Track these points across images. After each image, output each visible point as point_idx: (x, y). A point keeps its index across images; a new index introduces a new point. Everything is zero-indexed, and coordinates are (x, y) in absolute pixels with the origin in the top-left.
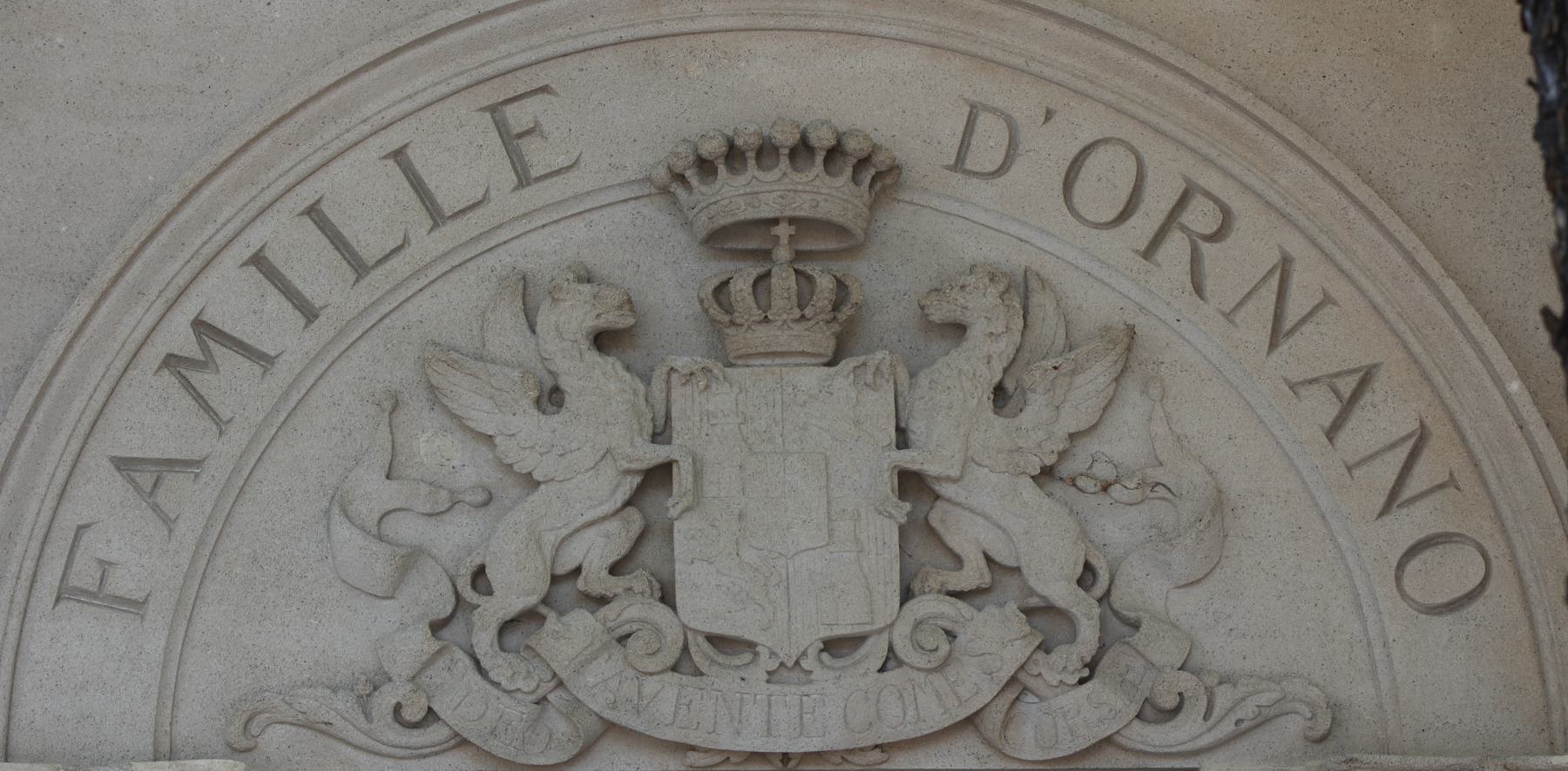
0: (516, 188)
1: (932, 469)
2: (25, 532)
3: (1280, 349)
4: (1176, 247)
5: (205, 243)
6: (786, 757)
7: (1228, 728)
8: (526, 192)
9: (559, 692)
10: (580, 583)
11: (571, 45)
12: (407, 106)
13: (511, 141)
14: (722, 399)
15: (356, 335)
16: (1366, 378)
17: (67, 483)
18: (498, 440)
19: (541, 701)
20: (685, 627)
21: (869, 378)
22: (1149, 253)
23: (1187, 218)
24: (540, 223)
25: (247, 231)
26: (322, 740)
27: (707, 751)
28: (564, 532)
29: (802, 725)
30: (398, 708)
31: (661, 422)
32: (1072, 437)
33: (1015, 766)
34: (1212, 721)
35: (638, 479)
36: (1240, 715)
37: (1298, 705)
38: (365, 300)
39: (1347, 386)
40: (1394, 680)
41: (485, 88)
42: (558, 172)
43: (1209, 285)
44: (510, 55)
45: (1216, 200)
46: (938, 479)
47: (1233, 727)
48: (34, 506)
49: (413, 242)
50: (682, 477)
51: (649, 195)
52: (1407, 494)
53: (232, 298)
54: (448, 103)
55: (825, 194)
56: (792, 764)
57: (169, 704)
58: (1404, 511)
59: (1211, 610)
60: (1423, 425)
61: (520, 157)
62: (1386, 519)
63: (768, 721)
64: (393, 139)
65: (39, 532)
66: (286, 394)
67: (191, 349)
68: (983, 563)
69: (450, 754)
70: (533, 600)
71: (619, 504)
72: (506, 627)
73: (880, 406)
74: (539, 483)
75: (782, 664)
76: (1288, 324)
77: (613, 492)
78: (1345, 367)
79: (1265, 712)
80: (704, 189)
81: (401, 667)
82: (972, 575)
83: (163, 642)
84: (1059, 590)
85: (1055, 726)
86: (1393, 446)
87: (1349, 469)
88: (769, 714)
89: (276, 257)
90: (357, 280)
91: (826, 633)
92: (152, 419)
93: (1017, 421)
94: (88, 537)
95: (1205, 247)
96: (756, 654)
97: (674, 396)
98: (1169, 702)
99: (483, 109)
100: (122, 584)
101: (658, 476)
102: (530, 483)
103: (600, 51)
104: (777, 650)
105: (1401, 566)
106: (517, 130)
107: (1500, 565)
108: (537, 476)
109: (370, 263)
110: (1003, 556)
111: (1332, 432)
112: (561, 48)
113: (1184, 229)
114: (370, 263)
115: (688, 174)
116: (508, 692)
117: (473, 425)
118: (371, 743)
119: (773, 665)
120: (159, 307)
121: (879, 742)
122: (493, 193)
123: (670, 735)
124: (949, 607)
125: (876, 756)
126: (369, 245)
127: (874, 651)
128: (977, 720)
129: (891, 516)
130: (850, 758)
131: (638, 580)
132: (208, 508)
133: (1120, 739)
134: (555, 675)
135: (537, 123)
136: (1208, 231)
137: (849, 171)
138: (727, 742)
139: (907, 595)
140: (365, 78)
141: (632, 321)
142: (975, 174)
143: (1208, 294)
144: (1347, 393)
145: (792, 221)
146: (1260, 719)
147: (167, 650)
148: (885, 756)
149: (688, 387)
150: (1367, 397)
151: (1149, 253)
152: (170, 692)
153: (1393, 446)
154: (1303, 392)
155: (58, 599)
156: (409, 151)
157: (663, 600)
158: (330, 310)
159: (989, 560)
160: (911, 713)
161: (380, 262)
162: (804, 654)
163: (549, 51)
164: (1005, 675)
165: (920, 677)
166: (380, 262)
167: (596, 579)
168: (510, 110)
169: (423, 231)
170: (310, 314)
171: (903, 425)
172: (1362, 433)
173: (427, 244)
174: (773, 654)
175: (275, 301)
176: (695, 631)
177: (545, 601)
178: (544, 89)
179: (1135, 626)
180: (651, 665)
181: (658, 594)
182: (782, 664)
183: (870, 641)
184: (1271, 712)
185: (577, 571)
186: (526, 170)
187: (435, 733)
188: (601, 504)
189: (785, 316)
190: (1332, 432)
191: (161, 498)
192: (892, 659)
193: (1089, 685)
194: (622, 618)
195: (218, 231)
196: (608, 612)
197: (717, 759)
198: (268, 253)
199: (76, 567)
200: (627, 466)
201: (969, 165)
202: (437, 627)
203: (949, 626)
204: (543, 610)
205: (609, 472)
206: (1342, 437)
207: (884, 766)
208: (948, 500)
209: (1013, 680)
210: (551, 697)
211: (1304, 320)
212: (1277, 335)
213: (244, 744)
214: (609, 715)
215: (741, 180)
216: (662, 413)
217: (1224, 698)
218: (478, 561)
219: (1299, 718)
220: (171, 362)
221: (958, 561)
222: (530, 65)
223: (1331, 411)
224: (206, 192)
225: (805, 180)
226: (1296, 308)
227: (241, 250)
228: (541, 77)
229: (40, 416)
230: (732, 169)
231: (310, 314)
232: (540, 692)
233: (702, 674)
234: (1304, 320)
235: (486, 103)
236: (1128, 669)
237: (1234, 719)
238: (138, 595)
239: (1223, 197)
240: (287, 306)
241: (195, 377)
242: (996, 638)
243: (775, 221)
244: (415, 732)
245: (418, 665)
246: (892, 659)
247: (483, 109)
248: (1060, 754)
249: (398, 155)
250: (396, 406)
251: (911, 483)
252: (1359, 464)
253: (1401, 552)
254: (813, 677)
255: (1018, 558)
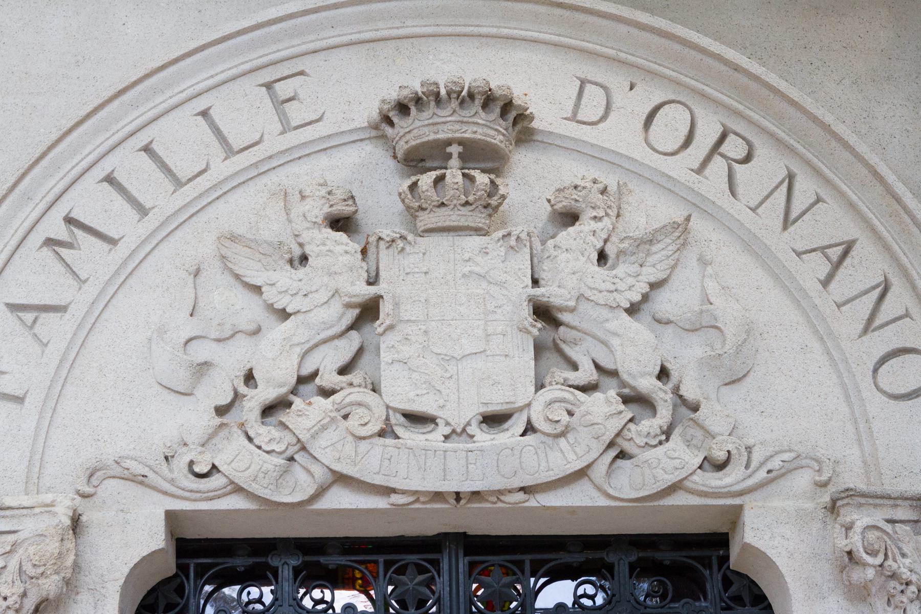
1: (556, 301)
3: (789, 230)
4: (718, 166)
5: (74, 167)
6: (458, 496)
7: (762, 475)
8: (288, 135)
9: (302, 453)
10: (318, 381)
12: (211, 82)
13: (280, 104)
15: (173, 227)
18: (263, 289)
19: (291, 459)
20: (388, 407)
22: (700, 170)
23: (724, 149)
24: (297, 156)
25: (102, 160)
26: (140, 490)
27: (404, 492)
28: (307, 346)
29: (468, 472)
30: (191, 463)
32: (654, 286)
34: (750, 470)
35: (357, 311)
36: (769, 466)
37: (808, 461)
38: (180, 203)
40: (874, 444)
42: (310, 123)
43: (740, 190)
44: (279, 51)
45: (744, 139)
47: (765, 475)
50: (385, 308)
51: (369, 138)
52: (877, 322)
53: (92, 202)
54: (238, 81)
55: (485, 128)
56: (463, 502)
57: (38, 465)
58: (876, 333)
59: (748, 399)
60: (886, 280)
61: (285, 114)
62: (864, 338)
63: (444, 470)
64: (201, 104)
67: (60, 231)
68: (593, 367)
69: (229, 497)
71: (344, 327)
73: (522, 262)
74: (290, 315)
75: (454, 431)
76: (793, 215)
77: (340, 318)
78: (832, 242)
82: (586, 374)
84: (647, 384)
86: (866, 292)
87: (839, 306)
88: (444, 464)
89: (120, 176)
91: (483, 409)
92: (35, 277)
93: (614, 272)
95: (736, 166)
96: (437, 424)
97: (381, 255)
98: (721, 455)
102: (284, 315)
103: (337, 50)
104: (450, 420)
105: (875, 371)
106: (284, 98)
108: (289, 310)
109: (184, 180)
113: (723, 156)
115: (391, 114)
116: (268, 452)
117: (247, 280)
118: (172, 489)
119: (447, 430)
120: (42, 206)
121: (522, 485)
122: (265, 137)
123: (378, 480)
125: (521, 496)
127: (518, 424)
129: (529, 332)
130: (502, 498)
131: (355, 377)
132: (69, 336)
133: (687, 483)
134: (299, 440)
136: (739, 157)
137: (498, 110)
139: (540, 386)
140: (182, 64)
141: (353, 209)
143: (740, 197)
146: (783, 470)
148: (526, 496)
149: (391, 250)
150: (848, 261)
151: (700, 170)
152: (38, 457)
153: (866, 292)
156: (211, 111)
157: (374, 390)
158: (156, 210)
159: (597, 367)
160: (543, 464)
161: (190, 180)
162: (469, 424)
163: (304, 48)
164: (607, 438)
165: (550, 441)
166: (190, 180)
167: (329, 378)
169: (220, 160)
170: (143, 211)
171: (536, 276)
172: (842, 286)
174: (447, 424)
175: (119, 201)
176: (395, 410)
177: (294, 392)
178: (302, 73)
179: (695, 408)
180: (364, 432)
181: (370, 387)
182: (454, 431)
183: (516, 415)
184: (794, 465)
185: (315, 374)
186: (288, 123)
187: (216, 481)
188: (331, 327)
189: (455, 202)
191: (37, 329)
192: (530, 429)
194: (345, 402)
195: (82, 159)
196: (336, 397)
197: (411, 499)
200: (347, 299)
201: (580, 117)
202: (221, 411)
203: (570, 407)
204: (292, 397)
205: (336, 307)
206: (833, 285)
207: (526, 504)
208: (568, 326)
209: (611, 444)
210: (296, 457)
211: (804, 213)
212: (787, 223)
213: (88, 490)
214: (337, 467)
215: (425, 115)
217: (757, 457)
218: (248, 367)
219: (809, 471)
220: (50, 242)
221: (575, 367)
222: (292, 58)
223: (826, 268)
224: (75, 134)
225: (468, 115)
226: (798, 206)
227: (100, 172)
228: (298, 65)
230: (420, 110)
231: (143, 211)
232: (289, 453)
233: (398, 438)
236: (693, 437)
238: (19, 393)
239: (749, 137)
242: (603, 407)
245: (206, 436)
246: (530, 429)
248: (647, 493)
249: (204, 114)
250: (197, 273)
251: (544, 313)
254: (475, 439)
255: (615, 363)
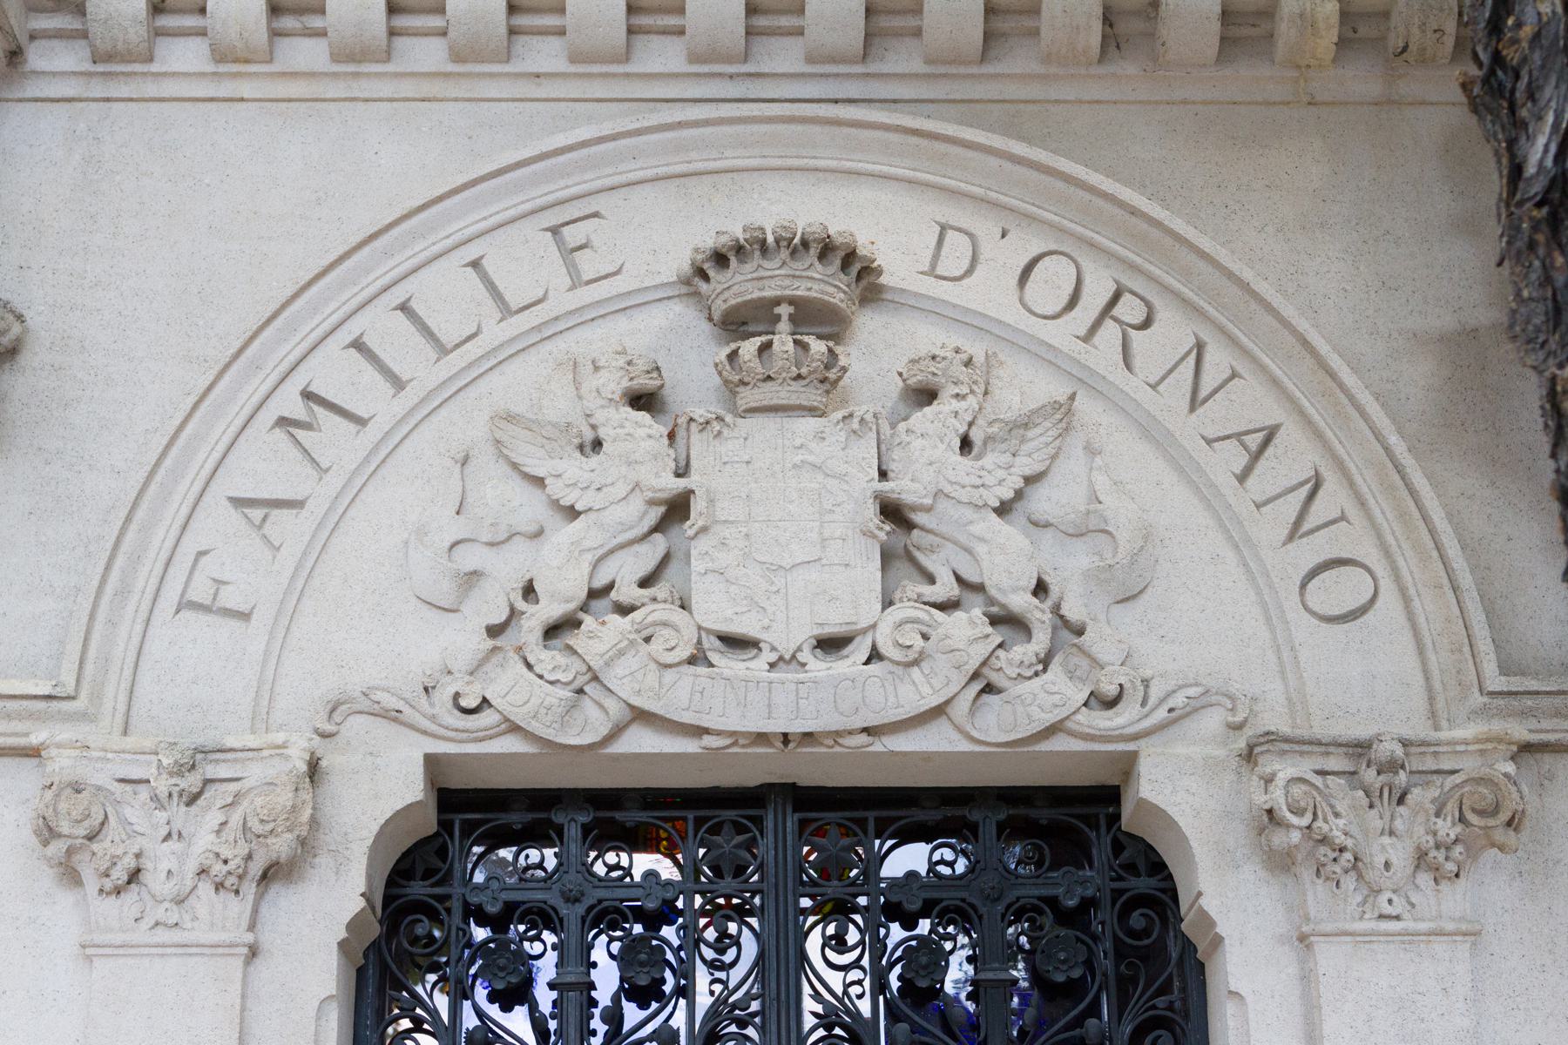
0: (570, 289)
1: (908, 498)
2: (152, 555)
4: (1110, 331)
7: (1161, 714)
8: (579, 291)
10: (613, 594)
11: (617, 180)
13: (570, 253)
14: (730, 447)
15: (436, 403)
16: (1270, 435)
17: (190, 517)
19: (580, 691)
21: (856, 426)
22: (1087, 338)
23: (1117, 311)
27: (719, 733)
30: (457, 696)
31: (683, 463)
32: (1030, 480)
33: (978, 748)
35: (662, 509)
36: (1171, 703)
39: (1254, 441)
41: (547, 213)
43: (1137, 362)
45: (1142, 299)
46: (914, 508)
48: (161, 533)
49: (484, 330)
50: (697, 506)
52: (1306, 527)
53: (336, 373)
54: (517, 224)
55: (821, 284)
57: (267, 697)
61: (575, 266)
62: (1289, 546)
64: (472, 252)
65: (164, 555)
66: (377, 447)
67: (297, 410)
70: (572, 606)
71: (646, 529)
72: (552, 631)
74: (579, 514)
76: (1203, 393)
78: (1251, 427)
79: (1193, 703)
80: (720, 277)
81: (461, 663)
82: (945, 588)
83: (262, 646)
84: (1021, 602)
85: (1015, 713)
90: (438, 360)
91: (818, 631)
92: (265, 465)
94: (204, 560)
95: (1132, 333)
99: (546, 230)
100: (229, 598)
101: (676, 509)
102: (572, 513)
104: (776, 644)
105: (1303, 586)
106: (572, 245)
107: (1386, 584)
108: (578, 507)
109: (449, 346)
110: (971, 575)
111: (1242, 477)
112: (608, 182)
113: (1116, 320)
114: (449, 346)
116: (551, 683)
118: (433, 728)
119: (773, 657)
123: (687, 718)
124: (923, 613)
125: (863, 739)
126: (449, 332)
127: (860, 650)
128: (949, 710)
129: (874, 537)
130: (840, 741)
131: (660, 590)
133: (1069, 724)
134: (590, 669)
135: (588, 240)
137: (838, 262)
138: (734, 723)
139: (887, 603)
141: (658, 383)
142: (945, 278)
143: (1137, 370)
144: (1254, 447)
145: (792, 301)
146: (1188, 709)
147: (267, 652)
148: (870, 739)
150: (1270, 451)
152: (267, 687)
154: (1216, 445)
155: (178, 611)
156: (484, 262)
157: (683, 607)
159: (959, 579)
160: (892, 699)
161: (457, 346)
162: (799, 649)
165: (899, 670)
166: (457, 346)
167: (626, 591)
168: (566, 230)
169: (493, 322)
170: (398, 384)
173: (496, 332)
174: (773, 649)
175: (370, 373)
176: (709, 631)
178: (596, 215)
179: (1080, 632)
180: (670, 658)
182: (781, 658)
186: (579, 276)
190: (1242, 477)
191: (267, 529)
192: (875, 656)
193: (1045, 677)
197: (728, 741)
198: (365, 339)
199: (193, 585)
201: (939, 271)
202: (494, 631)
203: (925, 629)
204: (581, 615)
205: (636, 505)
206: (1251, 481)
209: (975, 676)
210: (586, 689)
211: (1216, 391)
212: (1194, 403)
213: (329, 728)
215: (748, 267)
216: (684, 456)
221: (931, 579)
223: (1240, 461)
229: (168, 462)
231: (398, 384)
234: (1216, 391)
235: (547, 225)
237: (1166, 707)
238: (244, 608)
239: (1149, 297)
240: (378, 377)
241: (300, 434)
242: (966, 630)
243: (777, 302)
244: (471, 717)
246: (875, 656)
247: (546, 230)
249: (475, 264)
250: (465, 461)
251: (893, 512)
252: (1265, 503)
253: (1303, 574)
255: (982, 574)
